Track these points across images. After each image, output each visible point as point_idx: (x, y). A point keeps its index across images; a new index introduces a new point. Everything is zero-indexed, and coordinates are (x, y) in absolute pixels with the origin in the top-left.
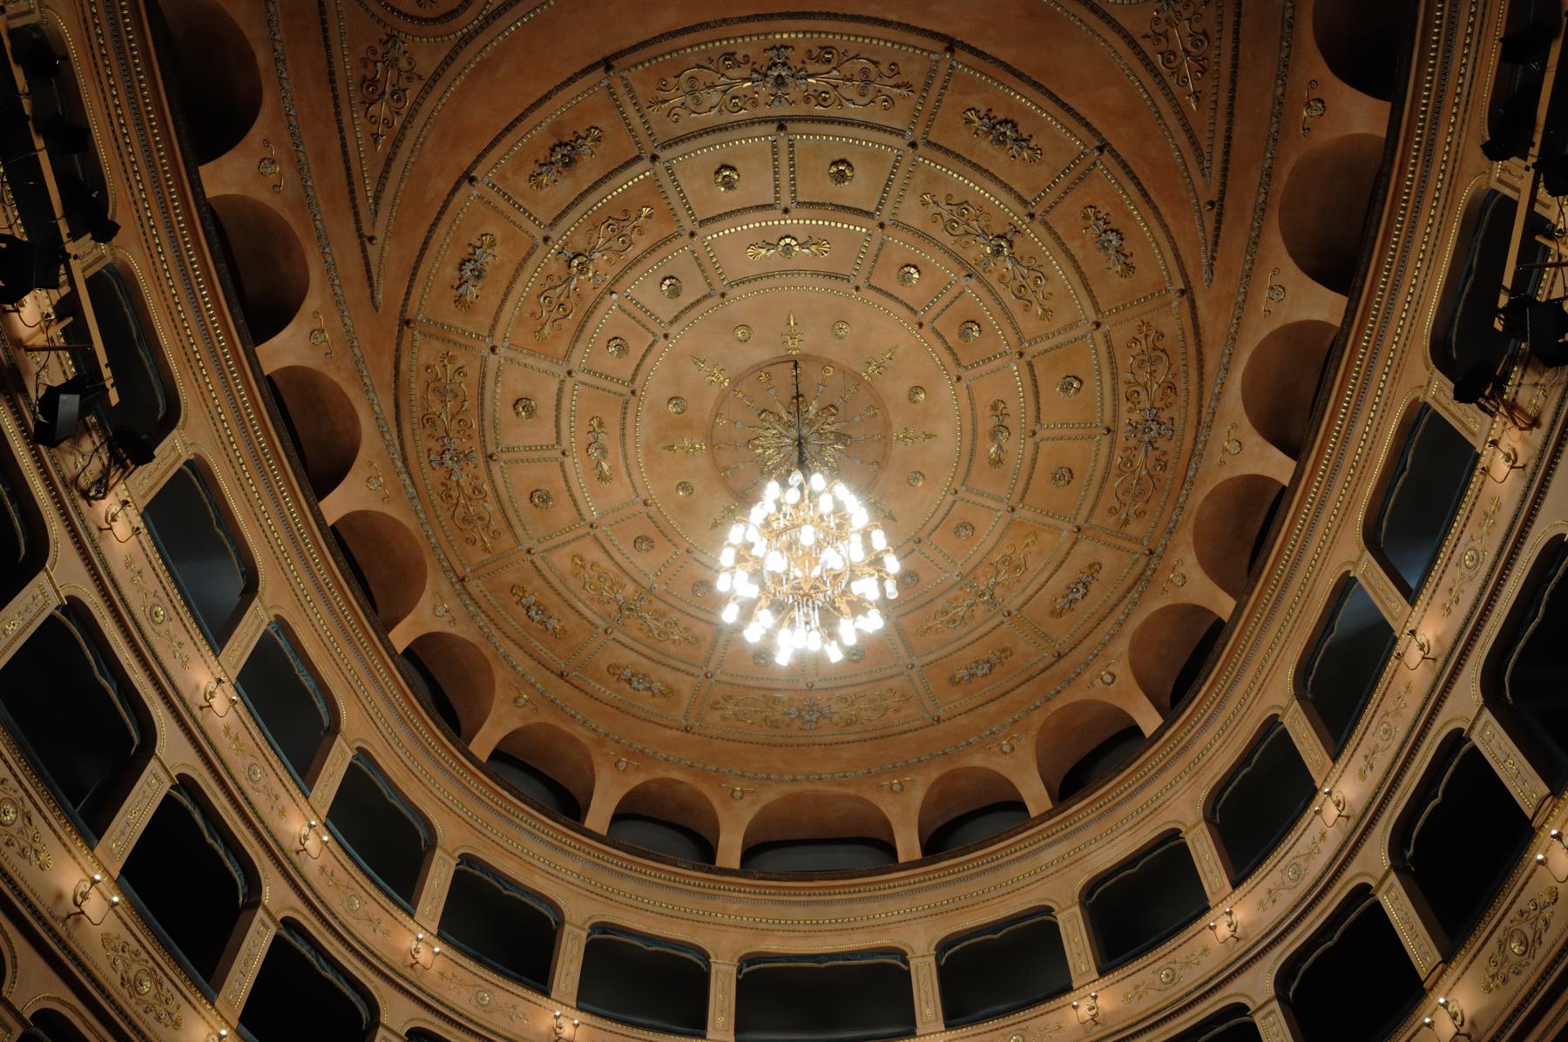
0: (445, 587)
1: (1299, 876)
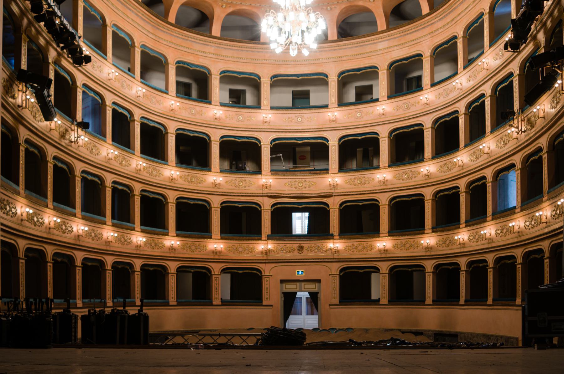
1: (447, 95)
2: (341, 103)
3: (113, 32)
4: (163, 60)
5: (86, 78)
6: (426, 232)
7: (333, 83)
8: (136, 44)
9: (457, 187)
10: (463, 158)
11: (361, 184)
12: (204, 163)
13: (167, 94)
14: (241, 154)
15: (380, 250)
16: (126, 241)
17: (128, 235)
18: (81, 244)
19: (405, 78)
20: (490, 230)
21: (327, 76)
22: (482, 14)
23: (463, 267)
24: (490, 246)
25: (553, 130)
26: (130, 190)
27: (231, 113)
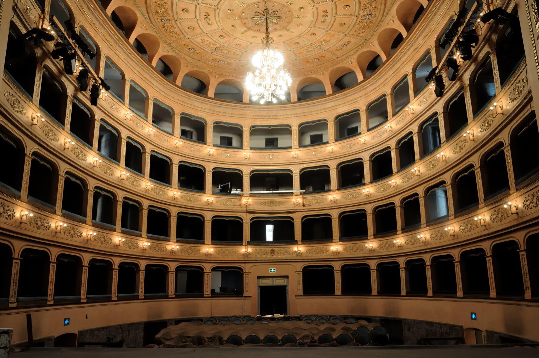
0: (165, 45)
1: (380, 136)
2: (301, 146)
3: (131, 85)
4: (171, 111)
5: (104, 115)
6: (369, 238)
7: (295, 131)
8: (150, 97)
9: (393, 203)
10: (395, 181)
11: (317, 203)
12: (200, 187)
13: (173, 135)
14: (227, 180)
15: (333, 253)
16: (133, 245)
17: (136, 241)
18: (89, 247)
19: (347, 127)
20: (424, 235)
21: (290, 127)
22: (406, 76)
23: (428, 262)
24: (426, 247)
25: (486, 148)
26: (139, 205)
27: (221, 152)
